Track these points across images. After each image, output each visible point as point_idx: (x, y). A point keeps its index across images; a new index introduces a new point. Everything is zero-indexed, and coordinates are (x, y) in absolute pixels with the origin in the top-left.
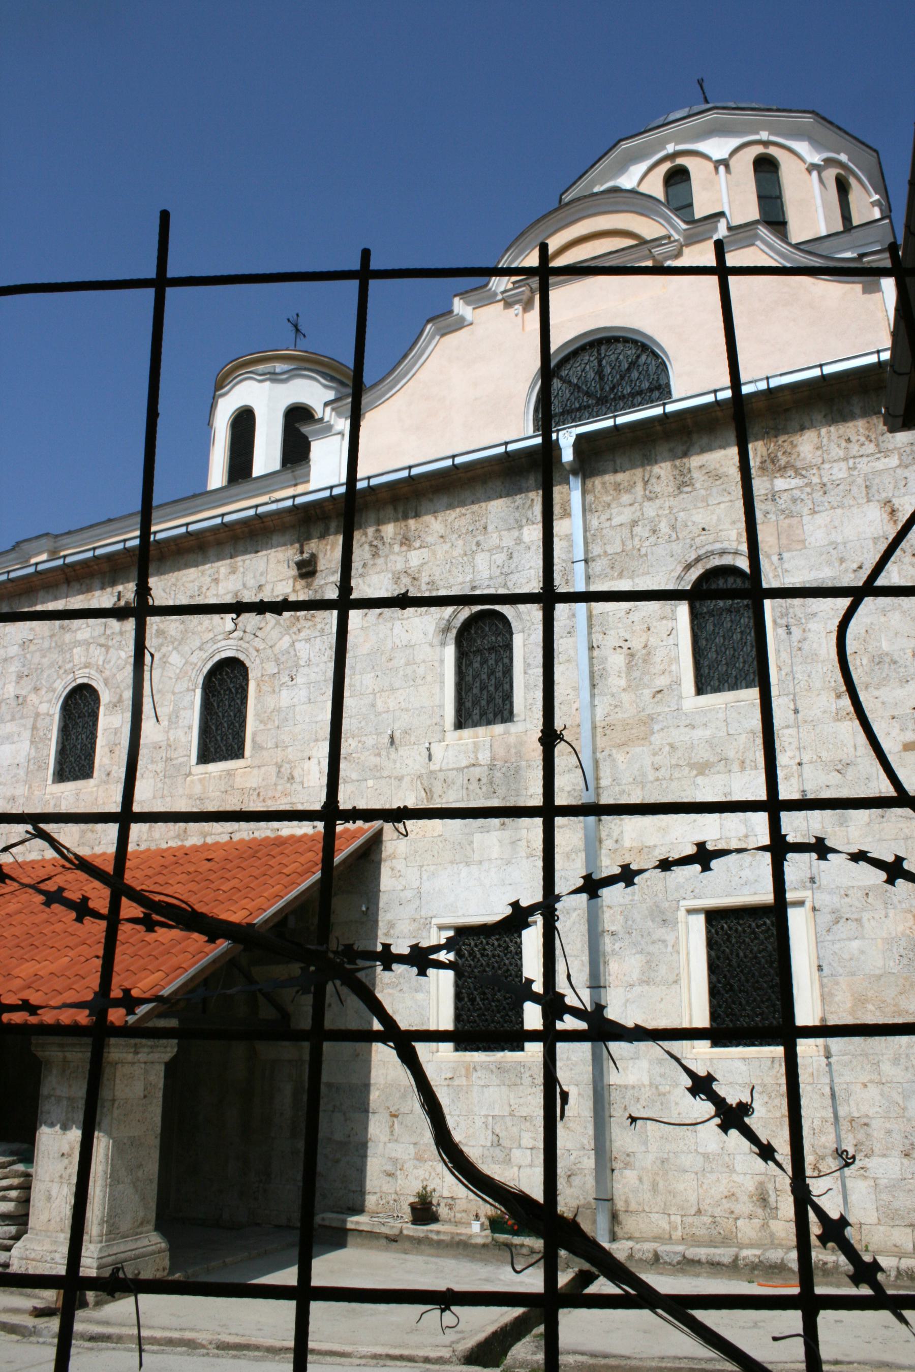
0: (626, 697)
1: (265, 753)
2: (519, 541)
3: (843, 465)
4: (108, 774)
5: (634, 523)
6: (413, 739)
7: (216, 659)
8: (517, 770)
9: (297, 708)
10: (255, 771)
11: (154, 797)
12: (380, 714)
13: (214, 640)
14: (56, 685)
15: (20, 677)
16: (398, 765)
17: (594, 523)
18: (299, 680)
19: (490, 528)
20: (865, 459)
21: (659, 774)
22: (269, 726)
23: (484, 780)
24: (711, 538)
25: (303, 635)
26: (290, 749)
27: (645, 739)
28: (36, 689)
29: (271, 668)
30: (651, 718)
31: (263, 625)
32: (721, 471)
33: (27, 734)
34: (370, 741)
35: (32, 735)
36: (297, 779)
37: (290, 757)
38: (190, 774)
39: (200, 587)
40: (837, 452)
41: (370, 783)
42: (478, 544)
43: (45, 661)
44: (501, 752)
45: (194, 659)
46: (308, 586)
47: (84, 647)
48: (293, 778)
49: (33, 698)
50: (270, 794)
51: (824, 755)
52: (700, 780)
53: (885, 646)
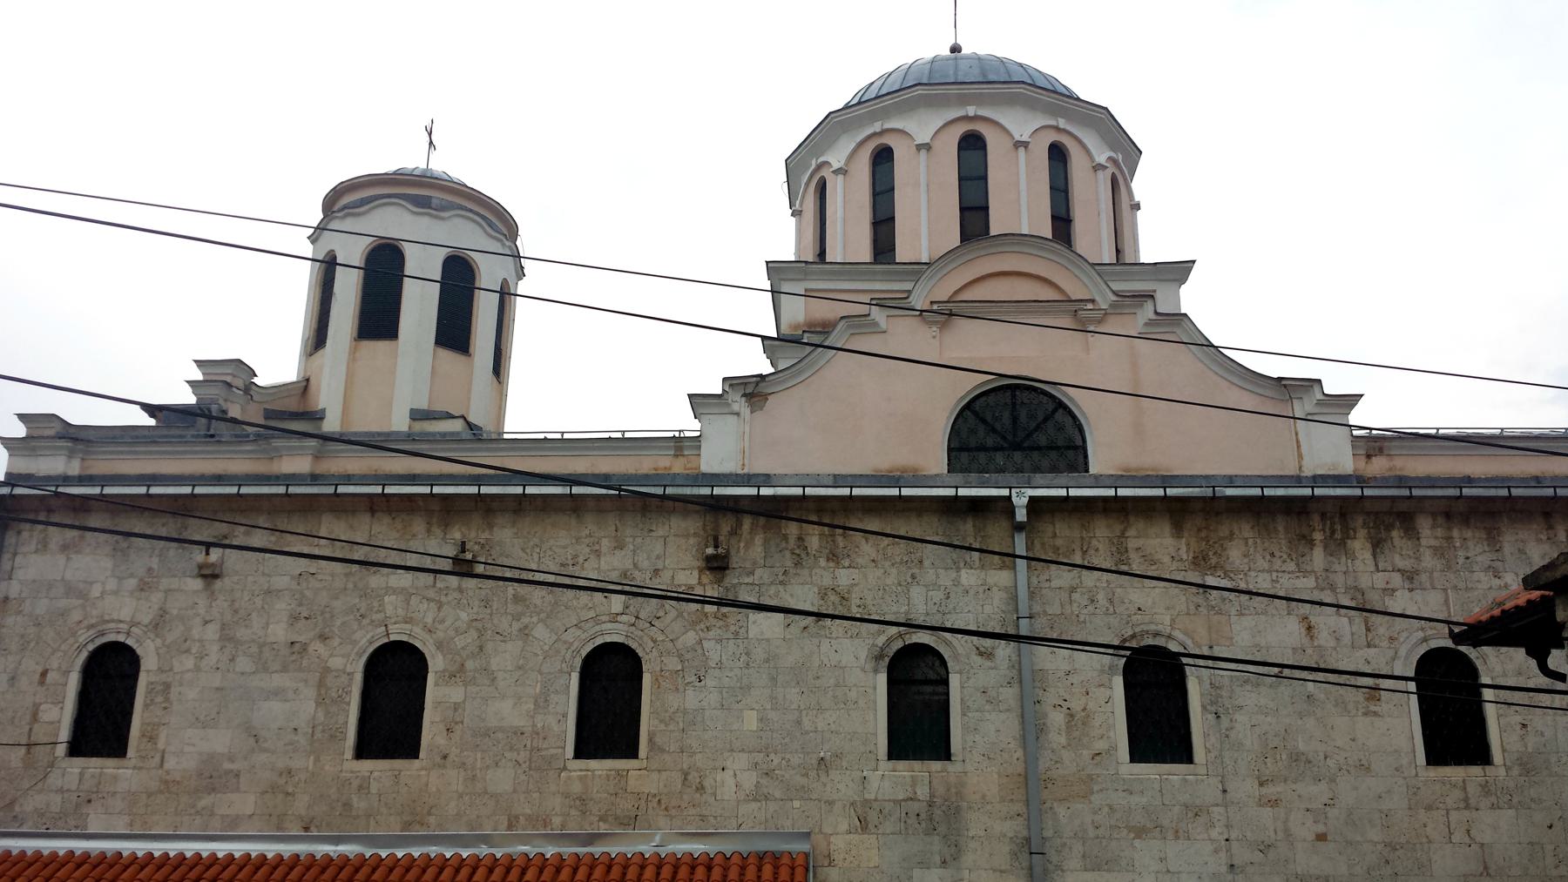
0: (1066, 755)
1: (667, 757)
2: (956, 582)
3: (1266, 575)
4: (445, 757)
5: (1073, 590)
6: (844, 764)
7: (599, 641)
8: (958, 810)
9: (707, 713)
10: (655, 775)
11: (515, 791)
12: (807, 733)
13: (596, 620)
14: (357, 636)
15: (294, 618)
16: (828, 788)
17: (1034, 580)
18: (709, 682)
19: (927, 563)
20: (1287, 576)
21: (1101, 832)
22: (671, 727)
23: (923, 816)
24: (1147, 619)
25: (712, 634)
26: (699, 756)
27: (1085, 797)
28: (323, 638)
29: (673, 664)
30: (1090, 777)
31: (661, 614)
32: (1156, 557)
33: (310, 693)
34: (796, 760)
35: (319, 694)
36: (709, 791)
37: (699, 764)
38: (565, 768)
39: (576, 556)
40: (1262, 563)
41: (797, 804)
42: (913, 577)
43: (337, 604)
44: (940, 790)
45: (568, 637)
46: (719, 581)
47: (401, 598)
48: (703, 788)
49: (317, 647)
50: (674, 803)
51: (1249, 834)
52: (1137, 843)
53: (1302, 747)
